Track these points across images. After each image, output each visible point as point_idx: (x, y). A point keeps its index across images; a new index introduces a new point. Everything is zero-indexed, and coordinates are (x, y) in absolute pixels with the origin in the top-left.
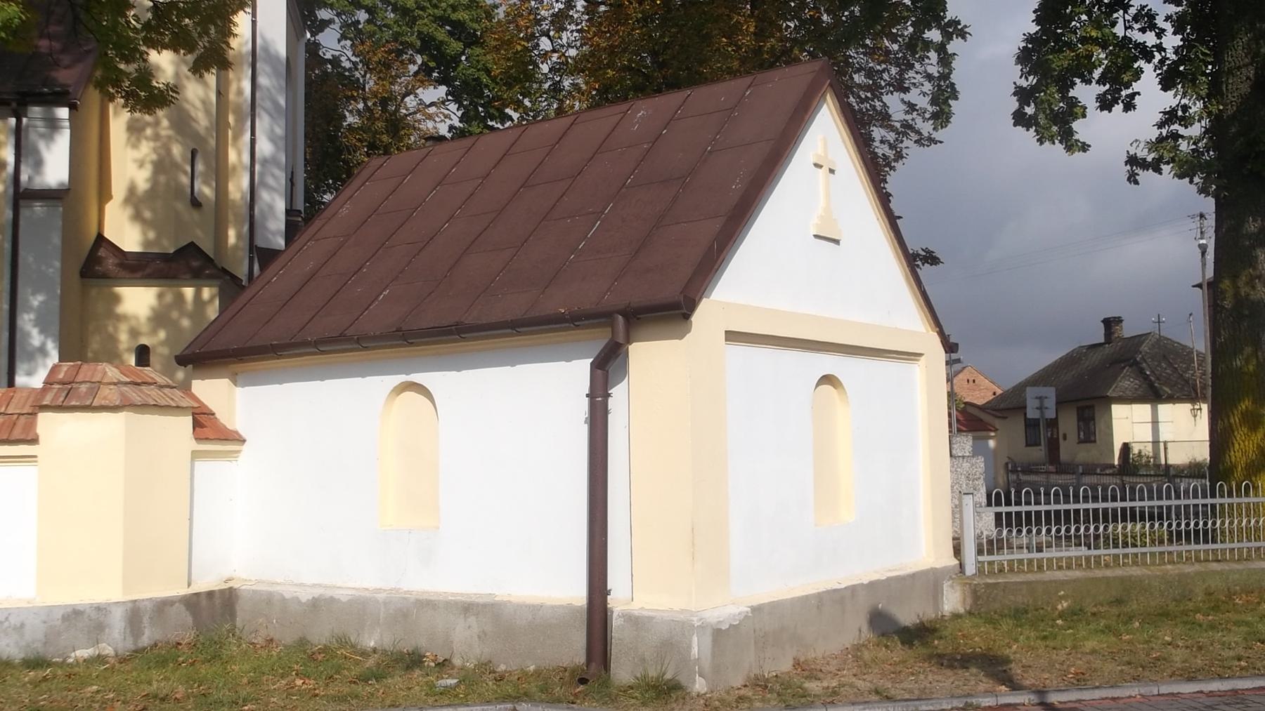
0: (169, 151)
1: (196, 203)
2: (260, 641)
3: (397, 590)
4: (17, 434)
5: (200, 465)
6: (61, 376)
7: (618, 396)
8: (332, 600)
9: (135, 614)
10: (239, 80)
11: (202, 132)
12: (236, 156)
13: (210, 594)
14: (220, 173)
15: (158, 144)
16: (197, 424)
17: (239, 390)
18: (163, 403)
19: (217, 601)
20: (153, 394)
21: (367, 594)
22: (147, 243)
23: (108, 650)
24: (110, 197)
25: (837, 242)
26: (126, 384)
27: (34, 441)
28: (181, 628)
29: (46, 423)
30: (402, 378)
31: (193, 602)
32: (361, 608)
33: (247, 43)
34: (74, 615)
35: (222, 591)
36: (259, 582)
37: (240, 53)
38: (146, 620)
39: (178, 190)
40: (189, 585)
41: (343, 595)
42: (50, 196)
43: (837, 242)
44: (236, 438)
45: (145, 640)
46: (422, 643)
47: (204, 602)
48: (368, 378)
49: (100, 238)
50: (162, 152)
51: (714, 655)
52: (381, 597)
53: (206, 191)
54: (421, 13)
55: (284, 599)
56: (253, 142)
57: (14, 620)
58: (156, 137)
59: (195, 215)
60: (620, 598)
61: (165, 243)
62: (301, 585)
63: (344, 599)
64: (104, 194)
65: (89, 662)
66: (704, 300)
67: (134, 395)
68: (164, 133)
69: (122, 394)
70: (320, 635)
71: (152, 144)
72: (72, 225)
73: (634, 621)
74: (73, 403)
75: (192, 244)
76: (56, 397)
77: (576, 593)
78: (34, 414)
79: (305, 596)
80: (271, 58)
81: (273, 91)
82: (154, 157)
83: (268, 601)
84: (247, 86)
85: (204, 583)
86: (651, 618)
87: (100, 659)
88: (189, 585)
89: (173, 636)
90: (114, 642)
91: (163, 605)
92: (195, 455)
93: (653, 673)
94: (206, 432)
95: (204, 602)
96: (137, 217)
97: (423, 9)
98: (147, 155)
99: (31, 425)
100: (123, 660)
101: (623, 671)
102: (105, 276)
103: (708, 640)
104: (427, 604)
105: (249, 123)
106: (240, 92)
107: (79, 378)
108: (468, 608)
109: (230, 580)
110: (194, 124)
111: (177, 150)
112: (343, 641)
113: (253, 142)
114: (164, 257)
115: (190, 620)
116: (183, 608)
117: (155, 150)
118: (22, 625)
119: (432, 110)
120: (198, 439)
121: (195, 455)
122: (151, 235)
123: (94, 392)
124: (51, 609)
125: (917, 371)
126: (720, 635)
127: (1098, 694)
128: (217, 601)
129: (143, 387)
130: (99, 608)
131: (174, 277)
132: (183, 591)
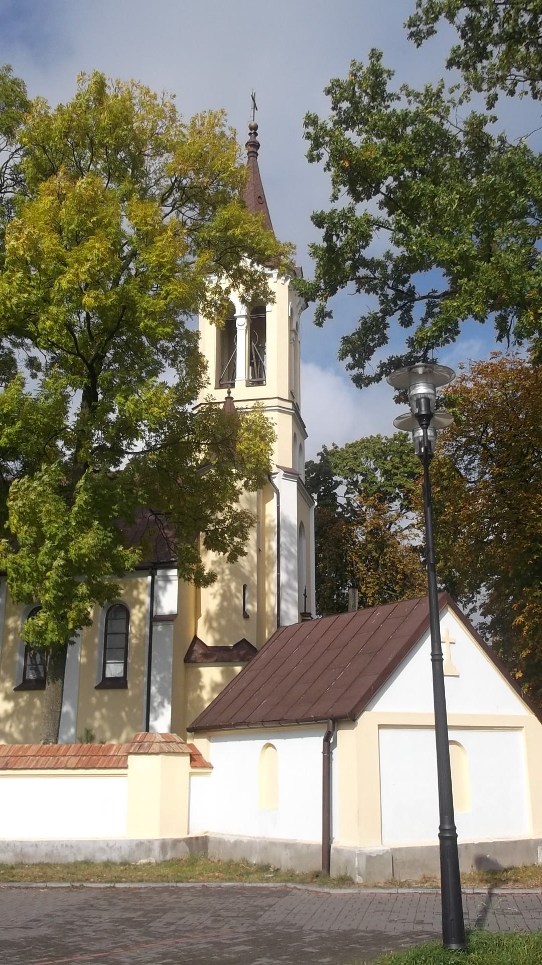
0: (229, 587)
1: (246, 616)
2: (216, 861)
3: (264, 838)
4: (120, 765)
5: (193, 778)
6: (138, 739)
7: (336, 753)
8: (241, 842)
9: (164, 845)
10: (269, 541)
11: (247, 573)
12: (271, 586)
13: (197, 838)
14: (261, 597)
15: (224, 584)
16: (192, 760)
17: (211, 744)
18: (177, 751)
19: (200, 842)
20: (174, 746)
21: (253, 839)
22: (215, 641)
23: (153, 861)
24: (201, 615)
25: (458, 676)
26: (163, 742)
27: (126, 768)
28: (183, 852)
29: (132, 760)
30: (265, 742)
31: (190, 842)
32: (250, 845)
33: (274, 521)
34: (140, 844)
35: (202, 837)
36: (218, 834)
37: (270, 525)
38: (168, 849)
39: (235, 609)
40: (188, 833)
41: (245, 840)
42: (168, 619)
43: (458, 676)
44: (208, 766)
45: (168, 857)
46: (271, 861)
47: (194, 842)
48: (242, 742)
49: (196, 638)
50: (226, 588)
51: (367, 866)
52: (258, 840)
53: (251, 607)
54: (396, 471)
55: (225, 841)
56: (279, 576)
57: (117, 845)
58: (223, 580)
59: (243, 622)
60: (340, 840)
61: (226, 640)
62: (232, 835)
63: (245, 841)
64: (197, 614)
65: (144, 865)
66: (365, 713)
67: (165, 747)
68: (226, 577)
69: (161, 747)
70: (237, 858)
71: (220, 584)
72: (179, 636)
73: (338, 851)
74: (141, 751)
75: (244, 640)
76: (135, 749)
77: (317, 838)
78: (127, 756)
79: (232, 840)
80: (289, 527)
81: (288, 545)
82: (221, 591)
83: (220, 842)
84: (274, 545)
85: (196, 832)
86: (343, 850)
87: (149, 864)
88: (188, 833)
89: (179, 856)
90: (155, 857)
91: (176, 842)
92: (191, 774)
93: (342, 874)
94: (196, 763)
95: (194, 842)
96: (211, 627)
97: (398, 468)
98: (217, 591)
99: (126, 760)
100: (158, 865)
101: (334, 874)
102: (195, 662)
103: (364, 861)
104: (273, 844)
105: (276, 568)
106: (270, 548)
107: (145, 740)
108: (287, 845)
109: (207, 832)
110: (242, 570)
111: (233, 586)
112: (244, 860)
113: (279, 576)
114: (226, 649)
115: (187, 849)
116: (184, 844)
117: (222, 587)
118: (121, 847)
119: (406, 532)
120: (192, 767)
121: (191, 774)
122: (217, 636)
123: (150, 746)
124: (131, 841)
125: (520, 735)
126: (370, 859)
127: (521, 891)
128: (200, 842)
129: (170, 744)
130: (150, 841)
131: (230, 661)
132: (186, 836)
